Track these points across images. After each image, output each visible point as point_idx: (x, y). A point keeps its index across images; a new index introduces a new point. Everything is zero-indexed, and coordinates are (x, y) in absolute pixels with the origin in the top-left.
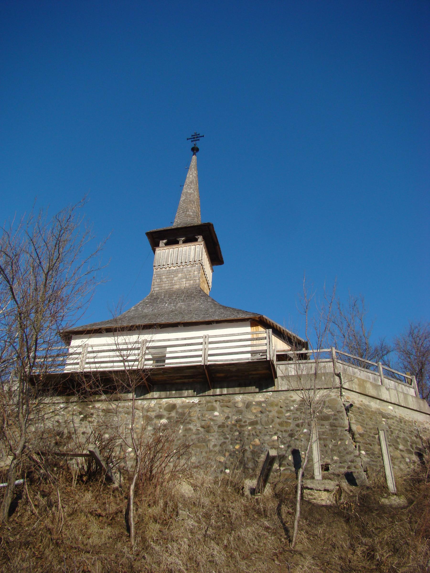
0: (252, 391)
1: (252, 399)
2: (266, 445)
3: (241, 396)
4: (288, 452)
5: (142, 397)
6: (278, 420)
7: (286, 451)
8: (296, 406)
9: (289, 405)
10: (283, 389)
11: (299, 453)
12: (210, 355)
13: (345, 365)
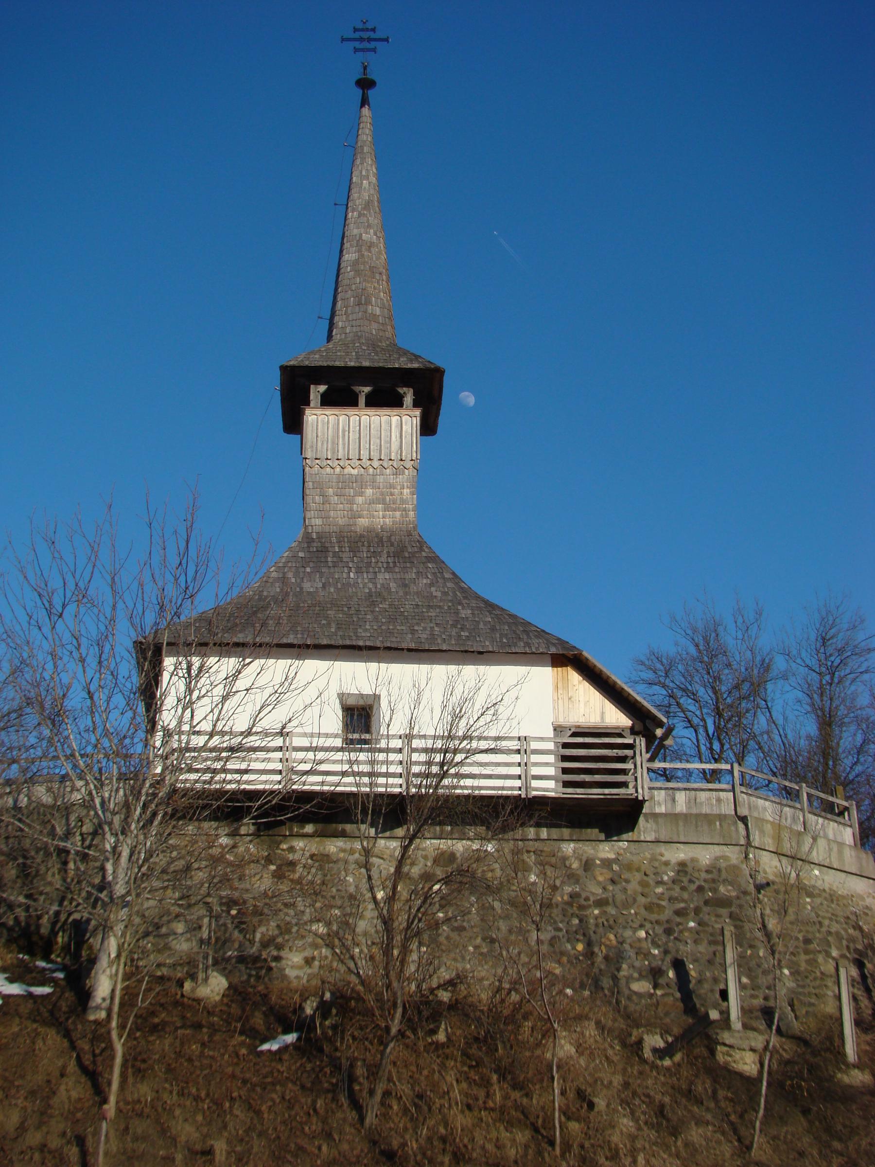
0: (593, 837)
1: (592, 852)
2: (627, 946)
3: (572, 845)
4: (665, 963)
5: (388, 834)
6: (642, 900)
7: (663, 960)
8: (672, 874)
9: (659, 870)
10: (648, 839)
11: (685, 965)
12: (536, 777)
13: (751, 795)
